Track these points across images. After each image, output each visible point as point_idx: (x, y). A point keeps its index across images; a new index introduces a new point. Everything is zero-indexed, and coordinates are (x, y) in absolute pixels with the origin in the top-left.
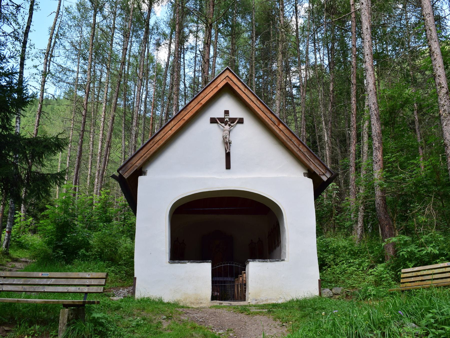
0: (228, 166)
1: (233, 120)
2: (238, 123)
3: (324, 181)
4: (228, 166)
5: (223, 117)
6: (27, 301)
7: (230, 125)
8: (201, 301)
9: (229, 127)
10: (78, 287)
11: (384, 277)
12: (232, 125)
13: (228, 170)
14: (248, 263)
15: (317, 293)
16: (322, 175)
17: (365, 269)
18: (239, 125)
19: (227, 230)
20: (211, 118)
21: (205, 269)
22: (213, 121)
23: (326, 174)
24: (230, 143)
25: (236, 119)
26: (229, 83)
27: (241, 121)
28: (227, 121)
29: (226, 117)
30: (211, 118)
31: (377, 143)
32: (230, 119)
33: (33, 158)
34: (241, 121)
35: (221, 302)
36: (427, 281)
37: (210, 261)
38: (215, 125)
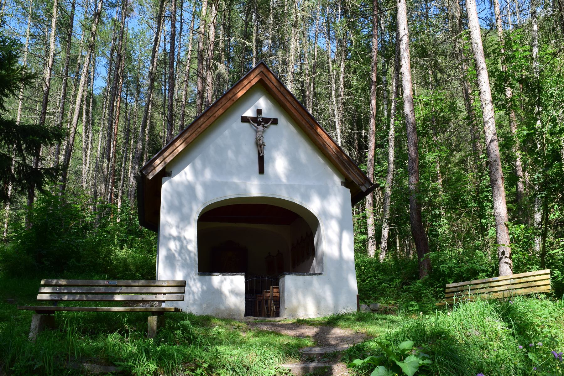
0: (261, 171)
1: (266, 120)
2: (272, 123)
3: (362, 191)
4: (261, 171)
5: (256, 116)
6: (109, 312)
7: (263, 126)
8: (235, 317)
9: (262, 128)
10: (155, 296)
11: (424, 293)
12: (266, 125)
13: (261, 175)
14: (284, 277)
15: (356, 309)
16: (361, 185)
17: (398, 285)
18: (273, 127)
19: (259, 241)
20: (277, 119)
21: (238, 282)
22: (245, 120)
23: (366, 185)
24: (264, 145)
25: (270, 119)
26: (264, 79)
27: (275, 122)
28: (260, 121)
29: (259, 116)
30: (277, 119)
31: (413, 153)
32: (263, 119)
33: (28, 149)
34: (275, 122)
35: (256, 318)
36: (541, 287)
37: (243, 273)
38: (246, 125)
